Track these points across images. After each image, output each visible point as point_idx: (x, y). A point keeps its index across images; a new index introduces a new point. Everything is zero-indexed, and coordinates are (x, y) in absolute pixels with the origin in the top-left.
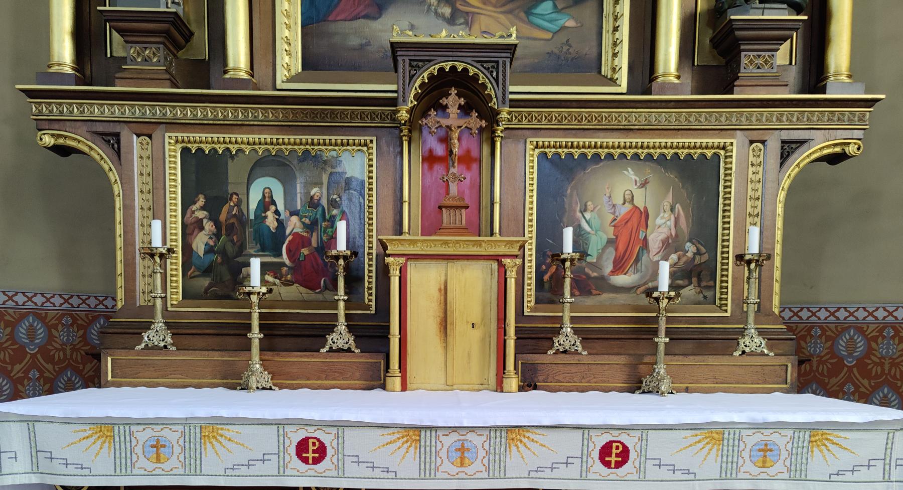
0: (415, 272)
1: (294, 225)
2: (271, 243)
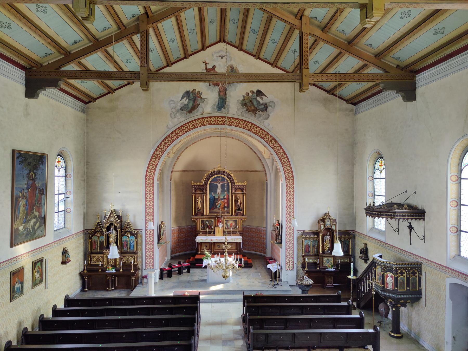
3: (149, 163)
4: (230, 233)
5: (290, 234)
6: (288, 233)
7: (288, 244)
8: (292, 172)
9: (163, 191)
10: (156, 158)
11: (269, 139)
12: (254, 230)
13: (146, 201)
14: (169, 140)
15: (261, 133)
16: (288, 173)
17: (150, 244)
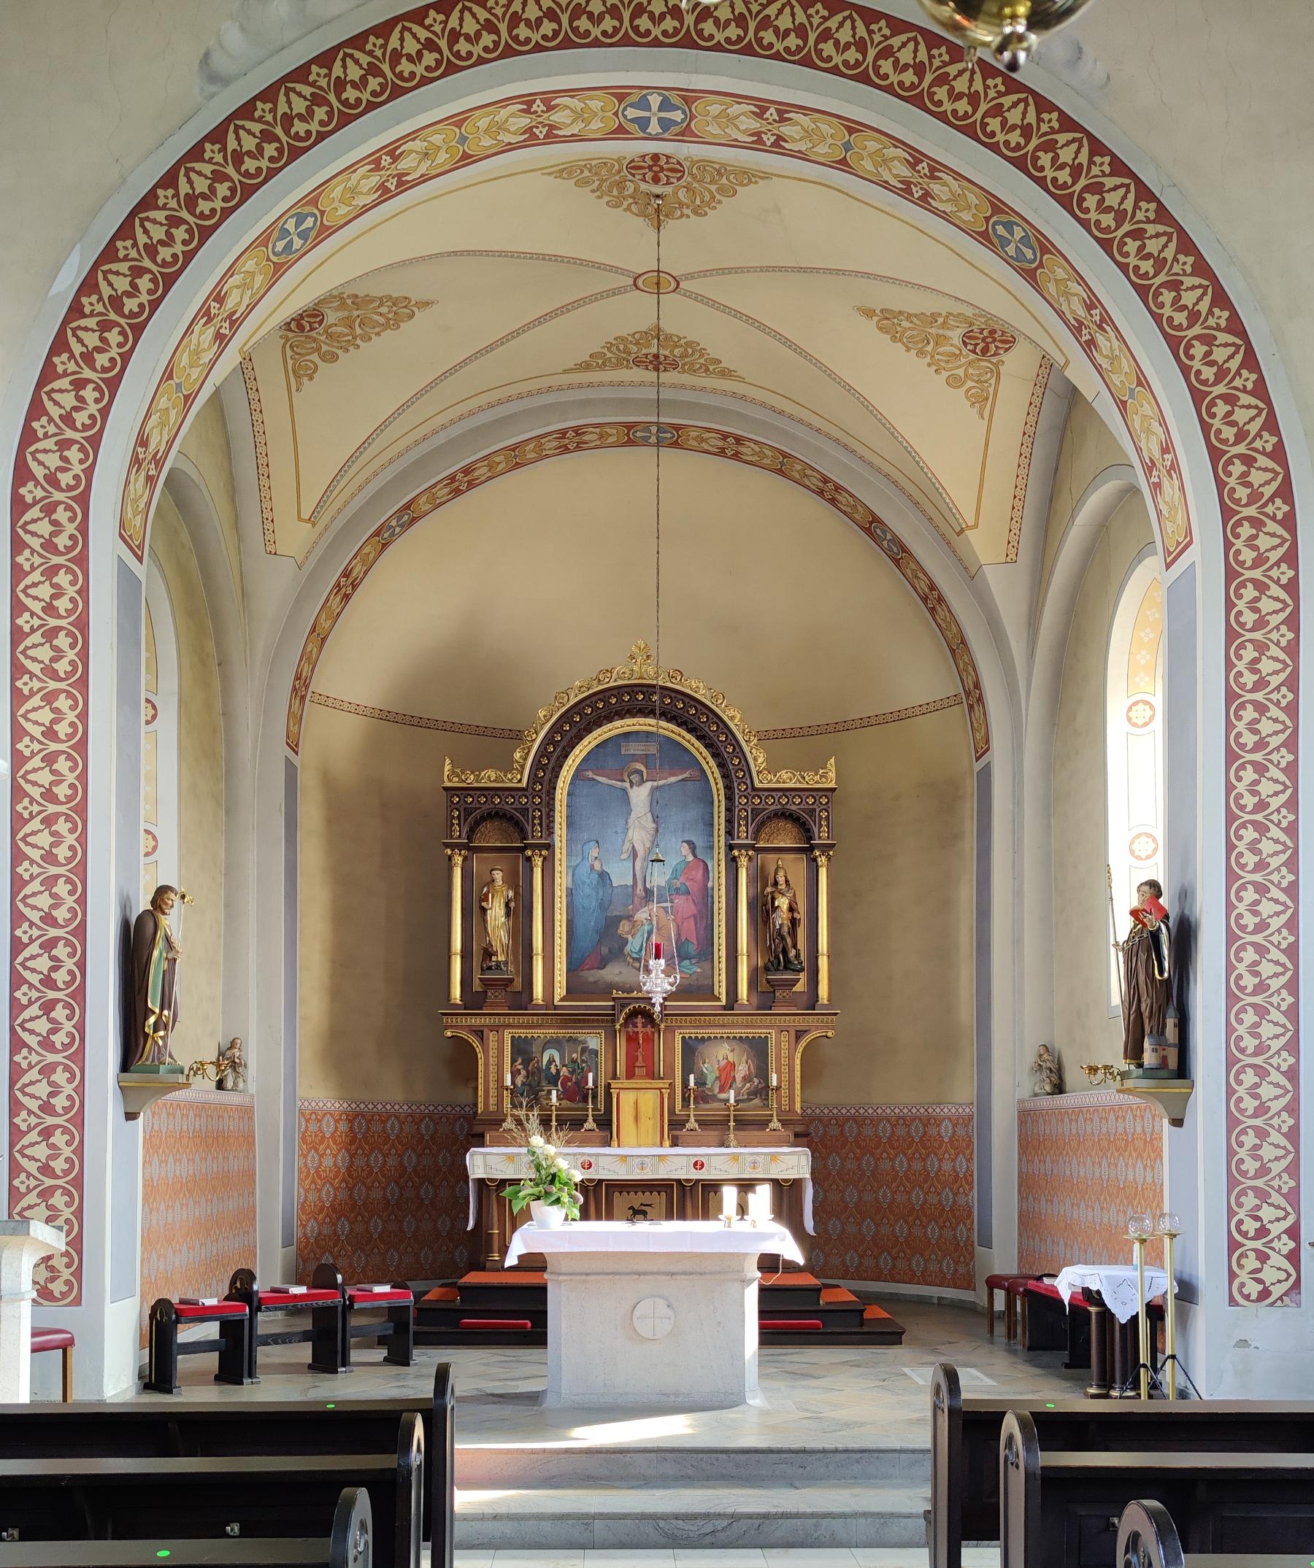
0: (624, 1095)
1: (564, 1071)
2: (553, 1080)
3: (48, 373)
4: (719, 1127)
5: (1261, 988)
6: (1249, 981)
7: (1249, 1078)
8: (1279, 454)
9: (228, 805)
10: (105, 326)
11: (1076, 171)
12: (885, 1130)
13: (18, 697)
14: (219, 177)
15: (1014, 117)
16: (1248, 461)
17: (48, 1070)
